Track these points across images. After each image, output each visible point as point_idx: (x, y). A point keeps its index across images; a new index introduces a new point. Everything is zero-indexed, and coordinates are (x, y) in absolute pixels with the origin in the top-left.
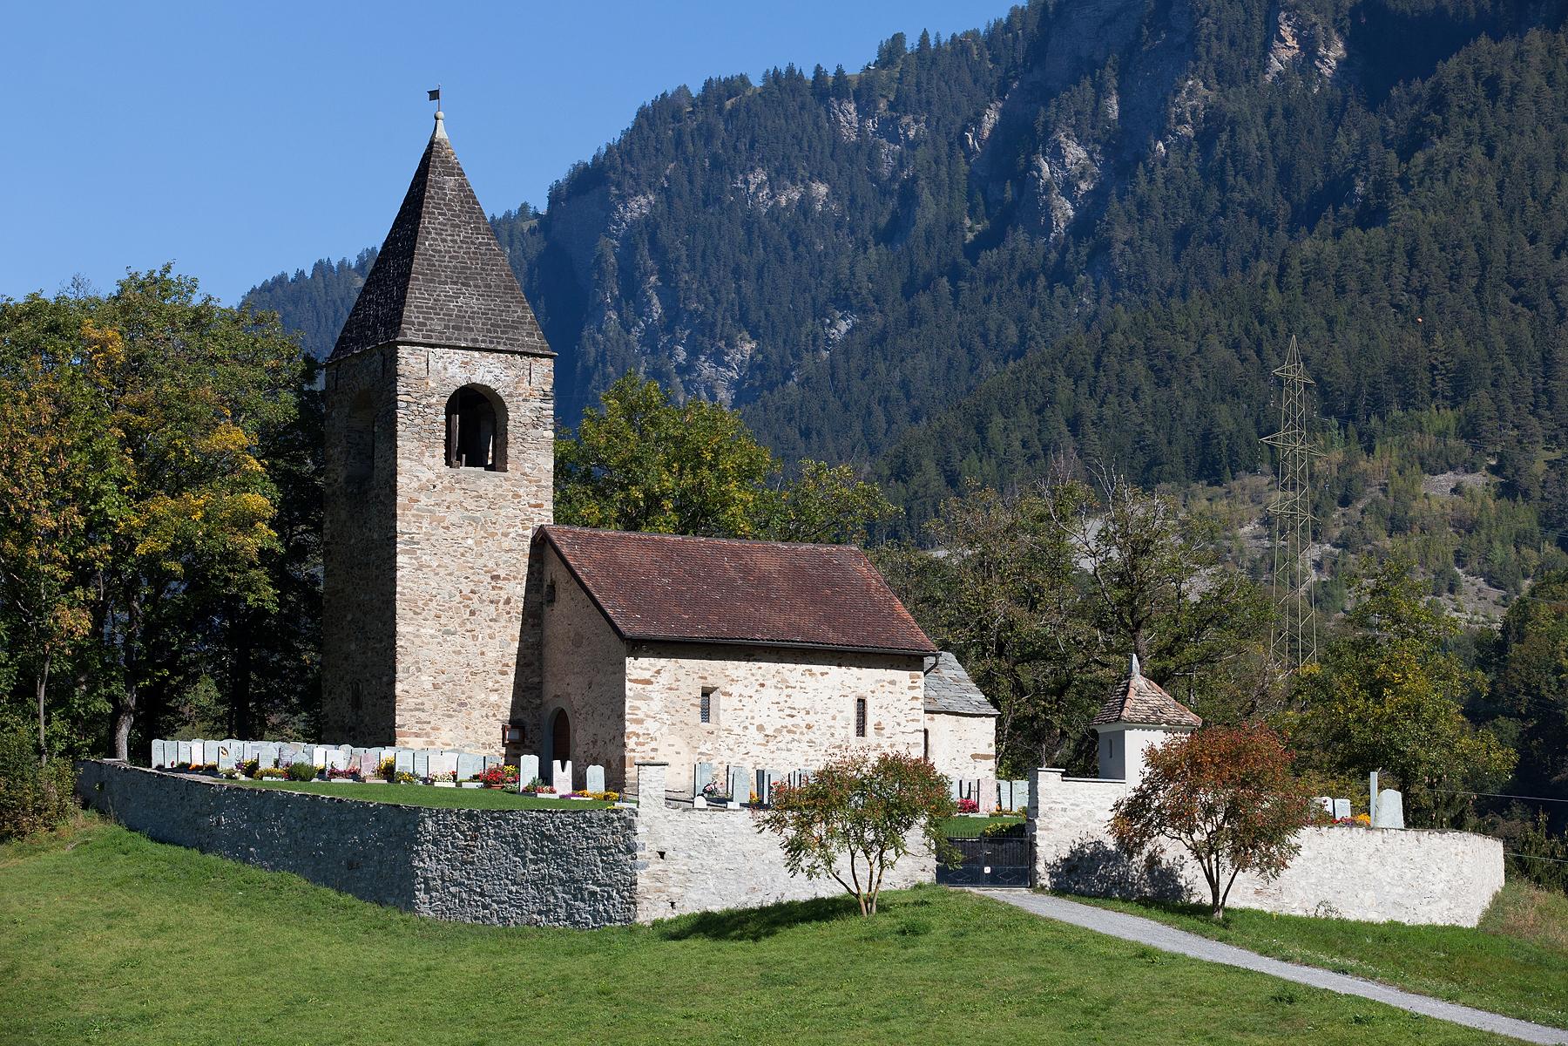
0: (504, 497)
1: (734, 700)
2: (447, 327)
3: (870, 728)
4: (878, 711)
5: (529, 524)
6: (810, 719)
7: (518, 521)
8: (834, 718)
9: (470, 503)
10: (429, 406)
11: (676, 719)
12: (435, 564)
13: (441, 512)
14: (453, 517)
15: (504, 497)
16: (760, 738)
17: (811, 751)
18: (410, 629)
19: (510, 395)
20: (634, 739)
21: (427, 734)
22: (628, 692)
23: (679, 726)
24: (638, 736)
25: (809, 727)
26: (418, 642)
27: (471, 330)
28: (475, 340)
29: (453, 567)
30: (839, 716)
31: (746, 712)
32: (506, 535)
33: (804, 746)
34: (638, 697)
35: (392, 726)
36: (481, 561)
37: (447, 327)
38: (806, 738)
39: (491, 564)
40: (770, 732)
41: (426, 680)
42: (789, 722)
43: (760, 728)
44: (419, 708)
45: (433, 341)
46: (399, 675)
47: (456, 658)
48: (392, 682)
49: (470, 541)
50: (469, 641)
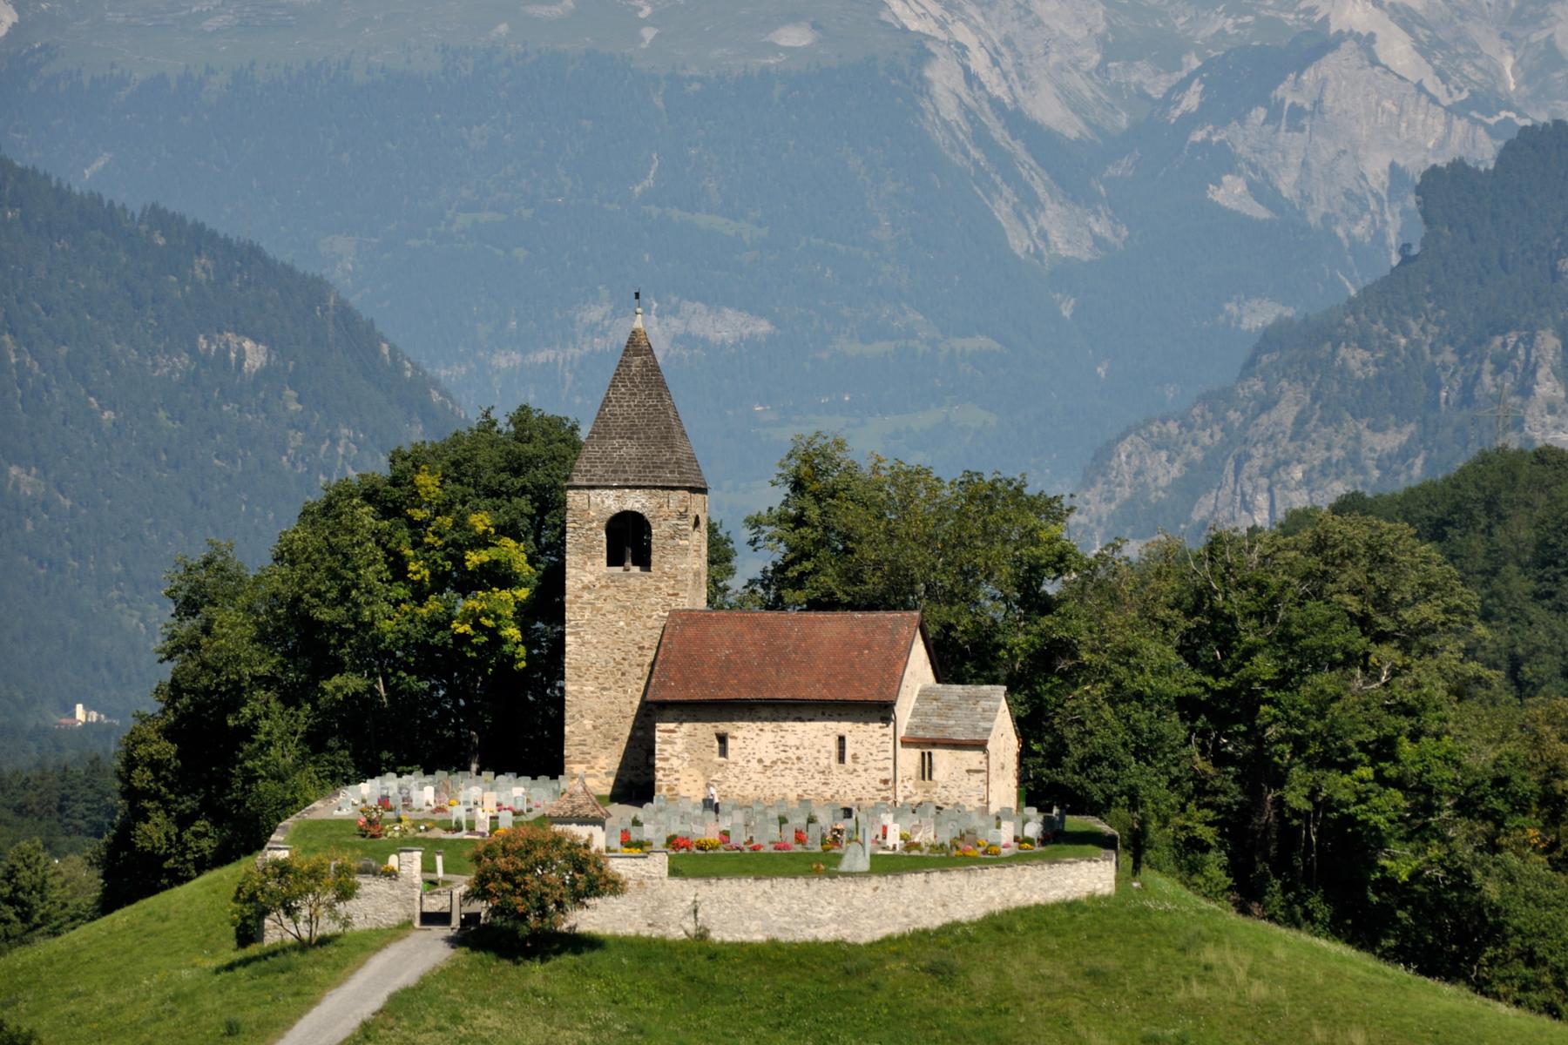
0: (647, 590)
1: (740, 743)
2: (607, 472)
3: (848, 758)
4: (854, 745)
5: (667, 608)
6: (799, 753)
7: (659, 607)
8: (819, 751)
9: (621, 596)
10: (591, 529)
11: (696, 755)
12: (595, 641)
13: (599, 604)
14: (609, 606)
15: (647, 590)
16: (759, 768)
17: (800, 777)
18: (576, 688)
19: (654, 517)
20: (662, 772)
21: (589, 762)
22: (657, 739)
23: (696, 762)
24: (664, 769)
25: (799, 758)
26: (580, 696)
27: (625, 472)
28: (627, 480)
29: (608, 642)
30: (823, 750)
31: (749, 750)
32: (649, 617)
33: (795, 772)
34: (665, 742)
35: (562, 757)
36: (630, 637)
37: (607, 472)
38: (796, 766)
39: (638, 638)
40: (768, 763)
41: (588, 724)
42: (783, 755)
43: (760, 761)
44: (583, 743)
45: (593, 483)
46: (567, 721)
47: (610, 707)
48: (562, 725)
49: (622, 623)
50: (621, 695)
